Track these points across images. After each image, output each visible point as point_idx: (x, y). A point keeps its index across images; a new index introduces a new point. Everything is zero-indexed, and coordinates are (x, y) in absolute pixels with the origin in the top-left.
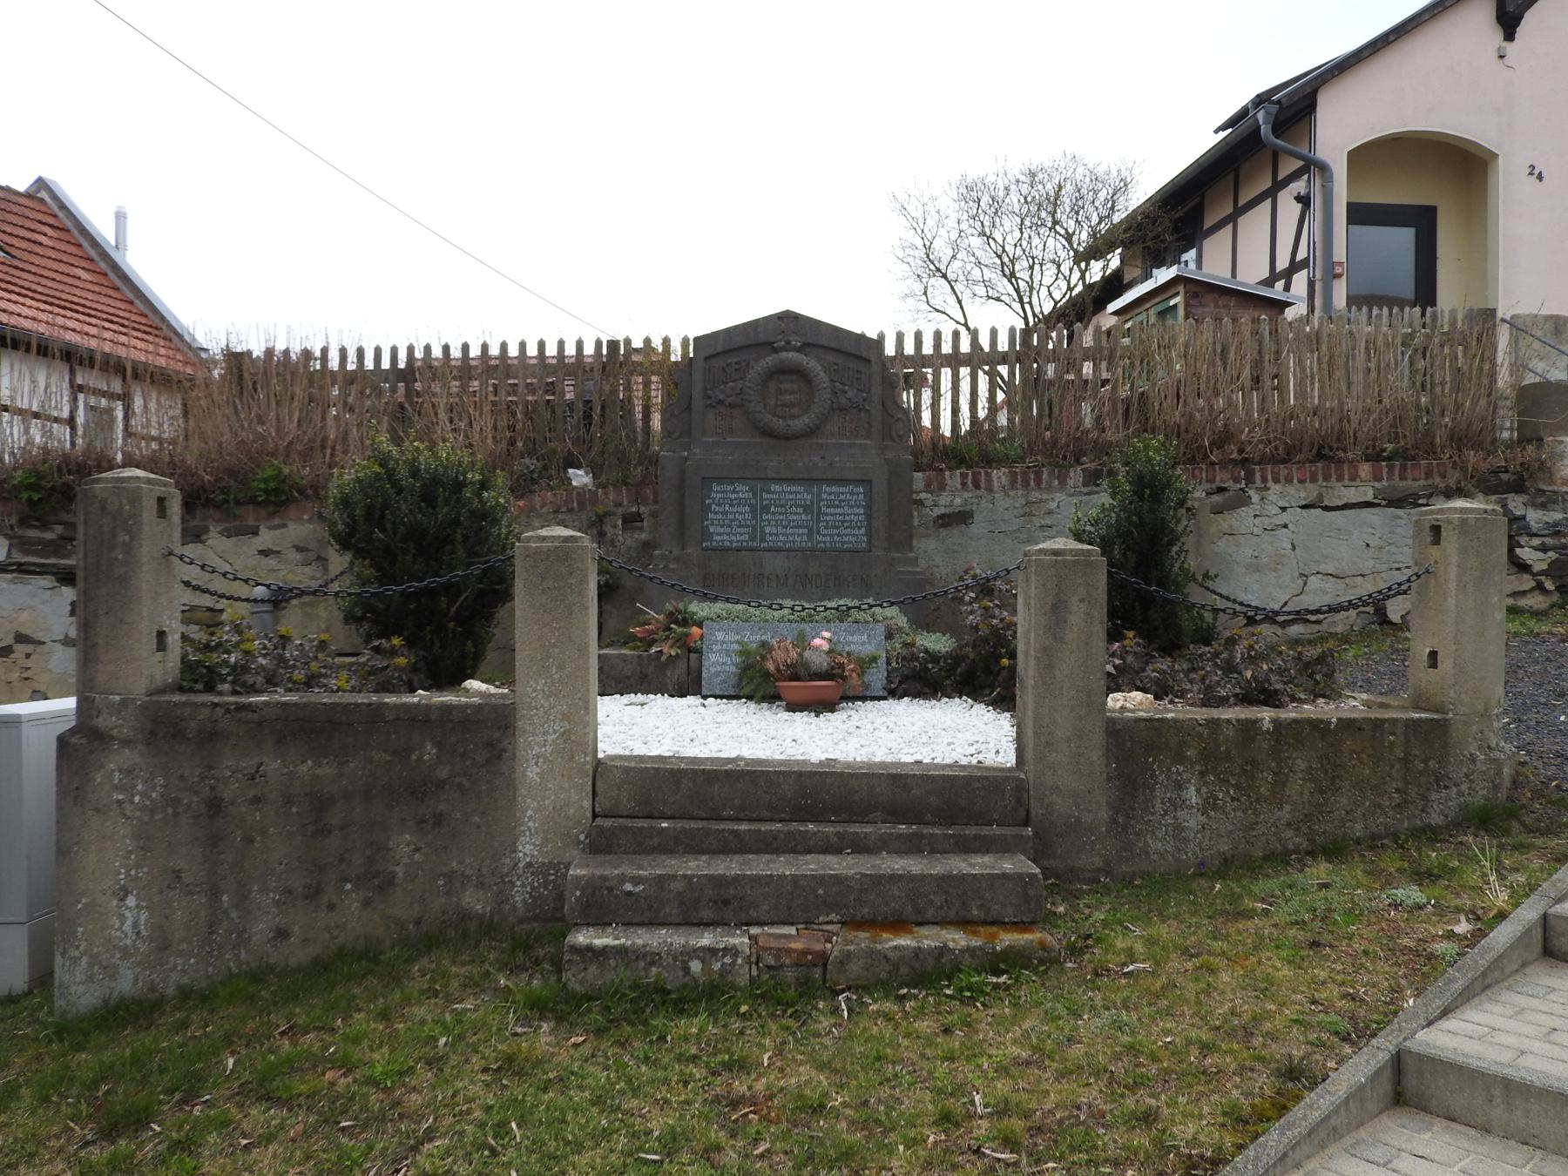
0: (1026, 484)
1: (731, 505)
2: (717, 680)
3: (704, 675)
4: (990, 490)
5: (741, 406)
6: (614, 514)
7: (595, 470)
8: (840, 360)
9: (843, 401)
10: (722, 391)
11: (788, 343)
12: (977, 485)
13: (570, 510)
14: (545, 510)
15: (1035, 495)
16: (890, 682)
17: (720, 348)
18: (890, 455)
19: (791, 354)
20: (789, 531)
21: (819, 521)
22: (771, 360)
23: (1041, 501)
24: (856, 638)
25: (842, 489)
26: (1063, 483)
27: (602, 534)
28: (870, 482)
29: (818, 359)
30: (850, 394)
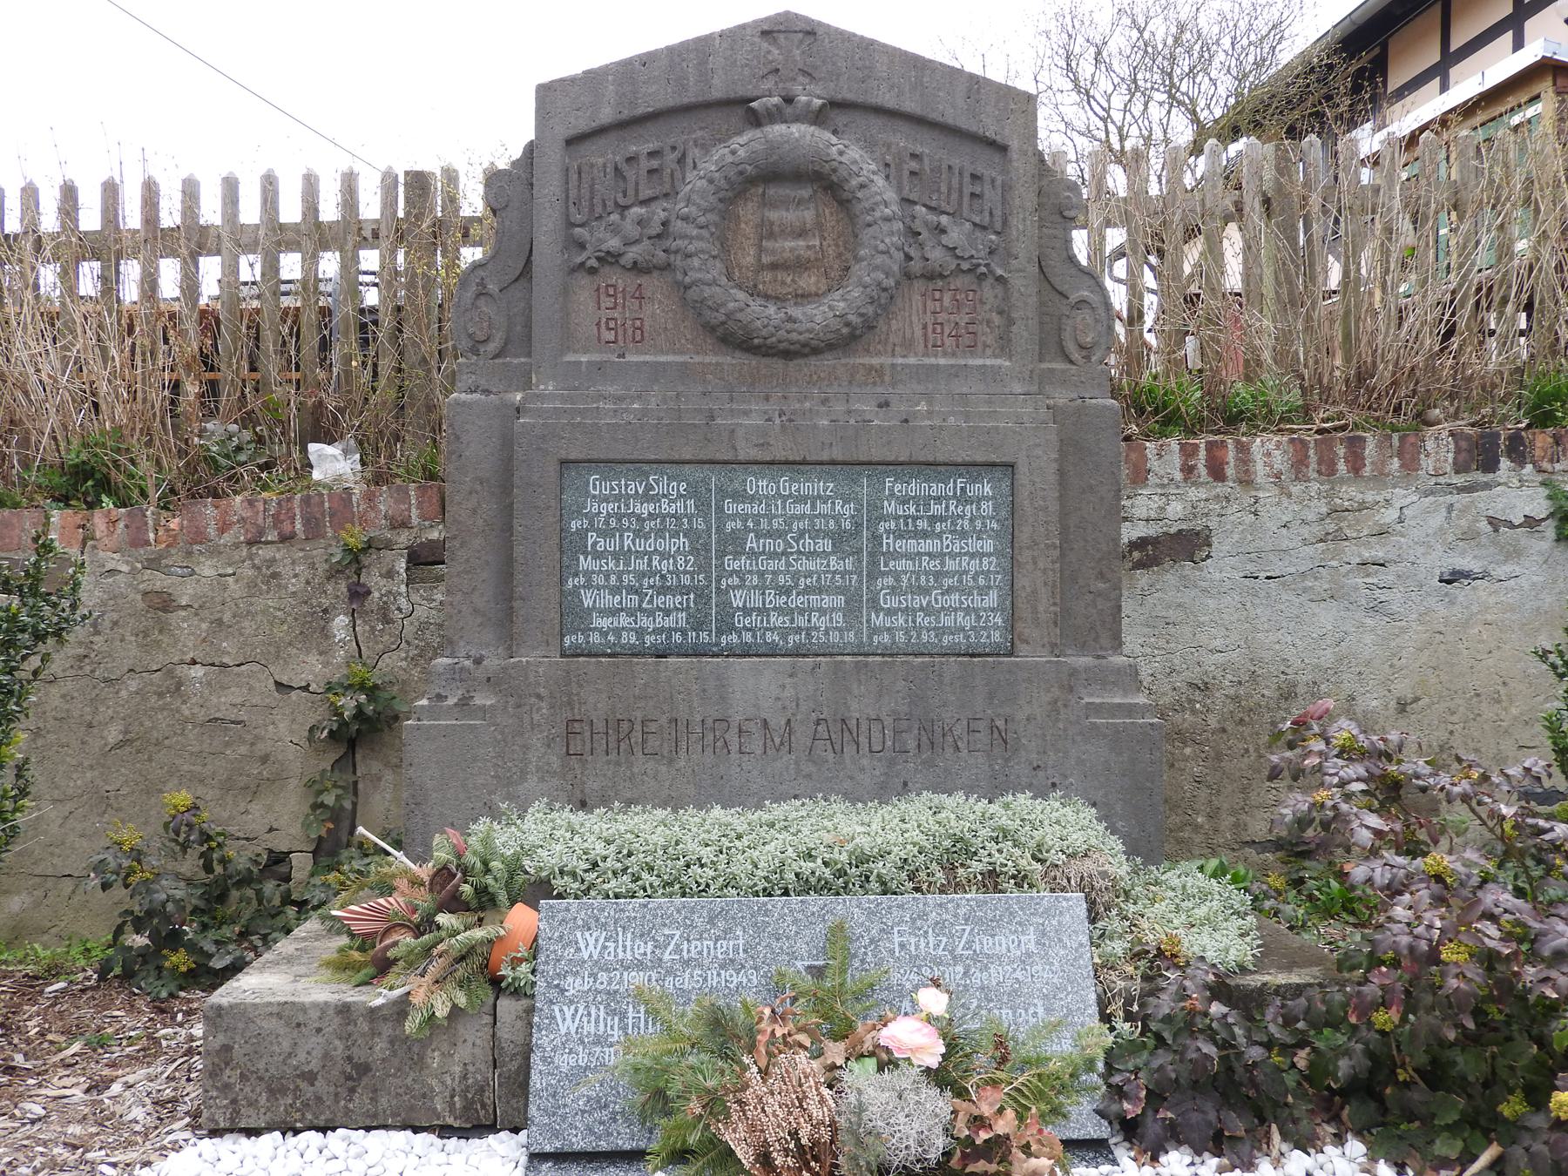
0: (1328, 468)
1: (638, 533)
2: (577, 1098)
3: (536, 1081)
4: (1246, 481)
5: (667, 267)
6: (389, 546)
7: (367, 449)
8: (927, 145)
9: (936, 255)
10: (615, 230)
11: (789, 100)
12: (1217, 473)
13: (286, 539)
14: (227, 538)
15: (1350, 493)
16: (1118, 1092)
17: (606, 115)
18: (1061, 397)
19: (797, 130)
20: (797, 601)
22: (745, 144)
23: (1363, 506)
24: (1003, 943)
25: (936, 489)
26: (1410, 465)
27: (358, 594)
29: (869, 145)
30: (956, 235)
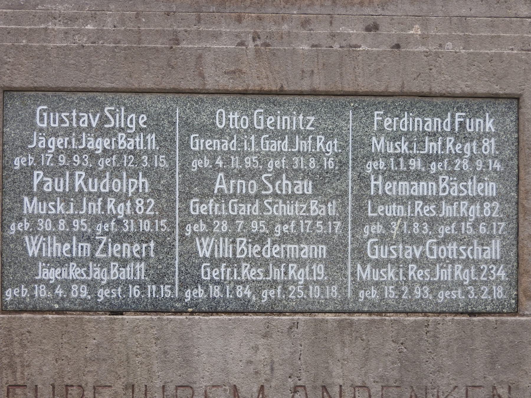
1: (92, 173)
20: (272, 251)
21: (360, 221)
25: (431, 124)
28: (517, 98)
